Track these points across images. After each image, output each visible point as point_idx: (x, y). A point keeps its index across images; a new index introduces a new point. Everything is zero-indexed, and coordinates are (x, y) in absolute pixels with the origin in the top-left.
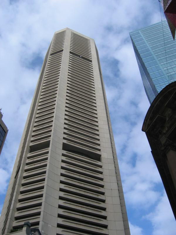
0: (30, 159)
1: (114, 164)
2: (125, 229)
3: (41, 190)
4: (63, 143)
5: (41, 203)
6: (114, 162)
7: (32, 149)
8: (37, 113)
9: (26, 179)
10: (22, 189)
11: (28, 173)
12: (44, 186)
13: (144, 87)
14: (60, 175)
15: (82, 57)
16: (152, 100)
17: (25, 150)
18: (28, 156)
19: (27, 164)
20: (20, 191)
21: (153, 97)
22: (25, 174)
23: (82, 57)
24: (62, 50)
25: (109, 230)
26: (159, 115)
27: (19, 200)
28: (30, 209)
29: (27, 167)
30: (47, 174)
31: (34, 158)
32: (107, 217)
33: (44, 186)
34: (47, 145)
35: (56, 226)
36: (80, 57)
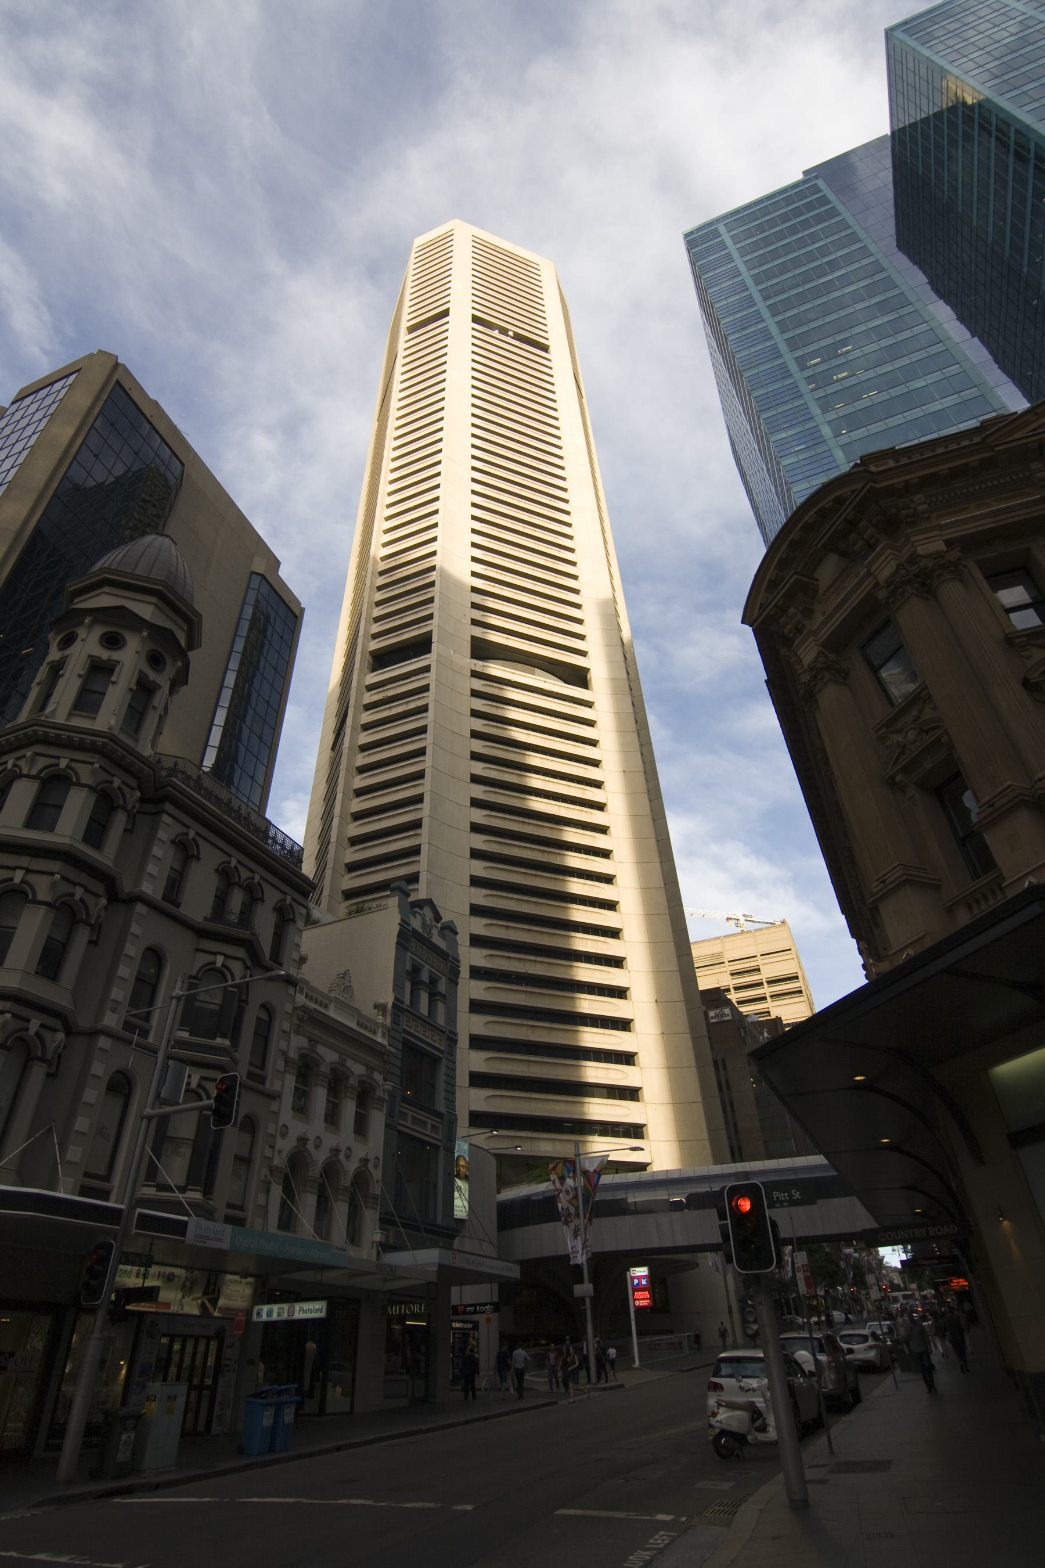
0: (373, 692)
1: (626, 663)
2: (665, 884)
3: (416, 783)
4: (473, 637)
5: (421, 819)
6: (629, 689)
7: (381, 659)
8: (373, 632)
9: (367, 753)
10: (360, 782)
11: (365, 777)
12: (424, 770)
13: (730, 435)
14: (469, 735)
15: (517, 337)
16: (773, 533)
17: (357, 666)
18: (372, 633)
19: (368, 707)
20: (359, 744)
21: (778, 520)
22: (365, 738)
23: (517, 337)
24: (446, 313)
25: (652, 1142)
26: (798, 577)
27: (360, 747)
28: (389, 839)
29: (367, 717)
30: (429, 735)
31: (385, 688)
32: (621, 930)
33: (424, 770)
34: (422, 645)
35: (469, 757)
36: (508, 336)
